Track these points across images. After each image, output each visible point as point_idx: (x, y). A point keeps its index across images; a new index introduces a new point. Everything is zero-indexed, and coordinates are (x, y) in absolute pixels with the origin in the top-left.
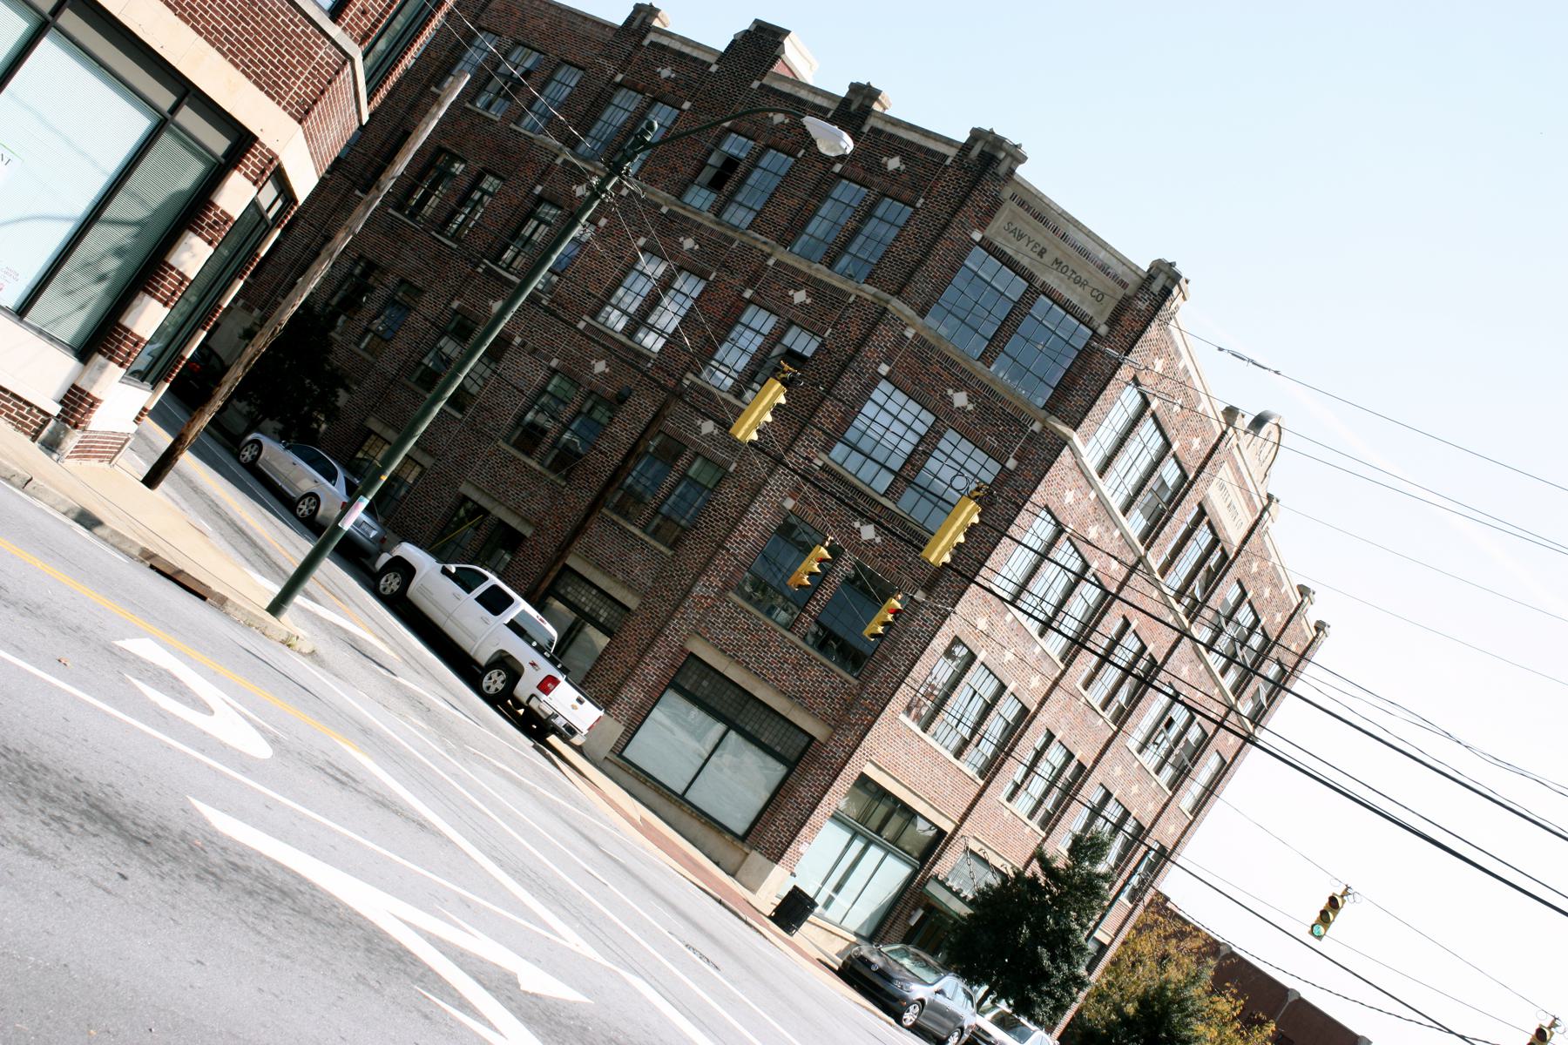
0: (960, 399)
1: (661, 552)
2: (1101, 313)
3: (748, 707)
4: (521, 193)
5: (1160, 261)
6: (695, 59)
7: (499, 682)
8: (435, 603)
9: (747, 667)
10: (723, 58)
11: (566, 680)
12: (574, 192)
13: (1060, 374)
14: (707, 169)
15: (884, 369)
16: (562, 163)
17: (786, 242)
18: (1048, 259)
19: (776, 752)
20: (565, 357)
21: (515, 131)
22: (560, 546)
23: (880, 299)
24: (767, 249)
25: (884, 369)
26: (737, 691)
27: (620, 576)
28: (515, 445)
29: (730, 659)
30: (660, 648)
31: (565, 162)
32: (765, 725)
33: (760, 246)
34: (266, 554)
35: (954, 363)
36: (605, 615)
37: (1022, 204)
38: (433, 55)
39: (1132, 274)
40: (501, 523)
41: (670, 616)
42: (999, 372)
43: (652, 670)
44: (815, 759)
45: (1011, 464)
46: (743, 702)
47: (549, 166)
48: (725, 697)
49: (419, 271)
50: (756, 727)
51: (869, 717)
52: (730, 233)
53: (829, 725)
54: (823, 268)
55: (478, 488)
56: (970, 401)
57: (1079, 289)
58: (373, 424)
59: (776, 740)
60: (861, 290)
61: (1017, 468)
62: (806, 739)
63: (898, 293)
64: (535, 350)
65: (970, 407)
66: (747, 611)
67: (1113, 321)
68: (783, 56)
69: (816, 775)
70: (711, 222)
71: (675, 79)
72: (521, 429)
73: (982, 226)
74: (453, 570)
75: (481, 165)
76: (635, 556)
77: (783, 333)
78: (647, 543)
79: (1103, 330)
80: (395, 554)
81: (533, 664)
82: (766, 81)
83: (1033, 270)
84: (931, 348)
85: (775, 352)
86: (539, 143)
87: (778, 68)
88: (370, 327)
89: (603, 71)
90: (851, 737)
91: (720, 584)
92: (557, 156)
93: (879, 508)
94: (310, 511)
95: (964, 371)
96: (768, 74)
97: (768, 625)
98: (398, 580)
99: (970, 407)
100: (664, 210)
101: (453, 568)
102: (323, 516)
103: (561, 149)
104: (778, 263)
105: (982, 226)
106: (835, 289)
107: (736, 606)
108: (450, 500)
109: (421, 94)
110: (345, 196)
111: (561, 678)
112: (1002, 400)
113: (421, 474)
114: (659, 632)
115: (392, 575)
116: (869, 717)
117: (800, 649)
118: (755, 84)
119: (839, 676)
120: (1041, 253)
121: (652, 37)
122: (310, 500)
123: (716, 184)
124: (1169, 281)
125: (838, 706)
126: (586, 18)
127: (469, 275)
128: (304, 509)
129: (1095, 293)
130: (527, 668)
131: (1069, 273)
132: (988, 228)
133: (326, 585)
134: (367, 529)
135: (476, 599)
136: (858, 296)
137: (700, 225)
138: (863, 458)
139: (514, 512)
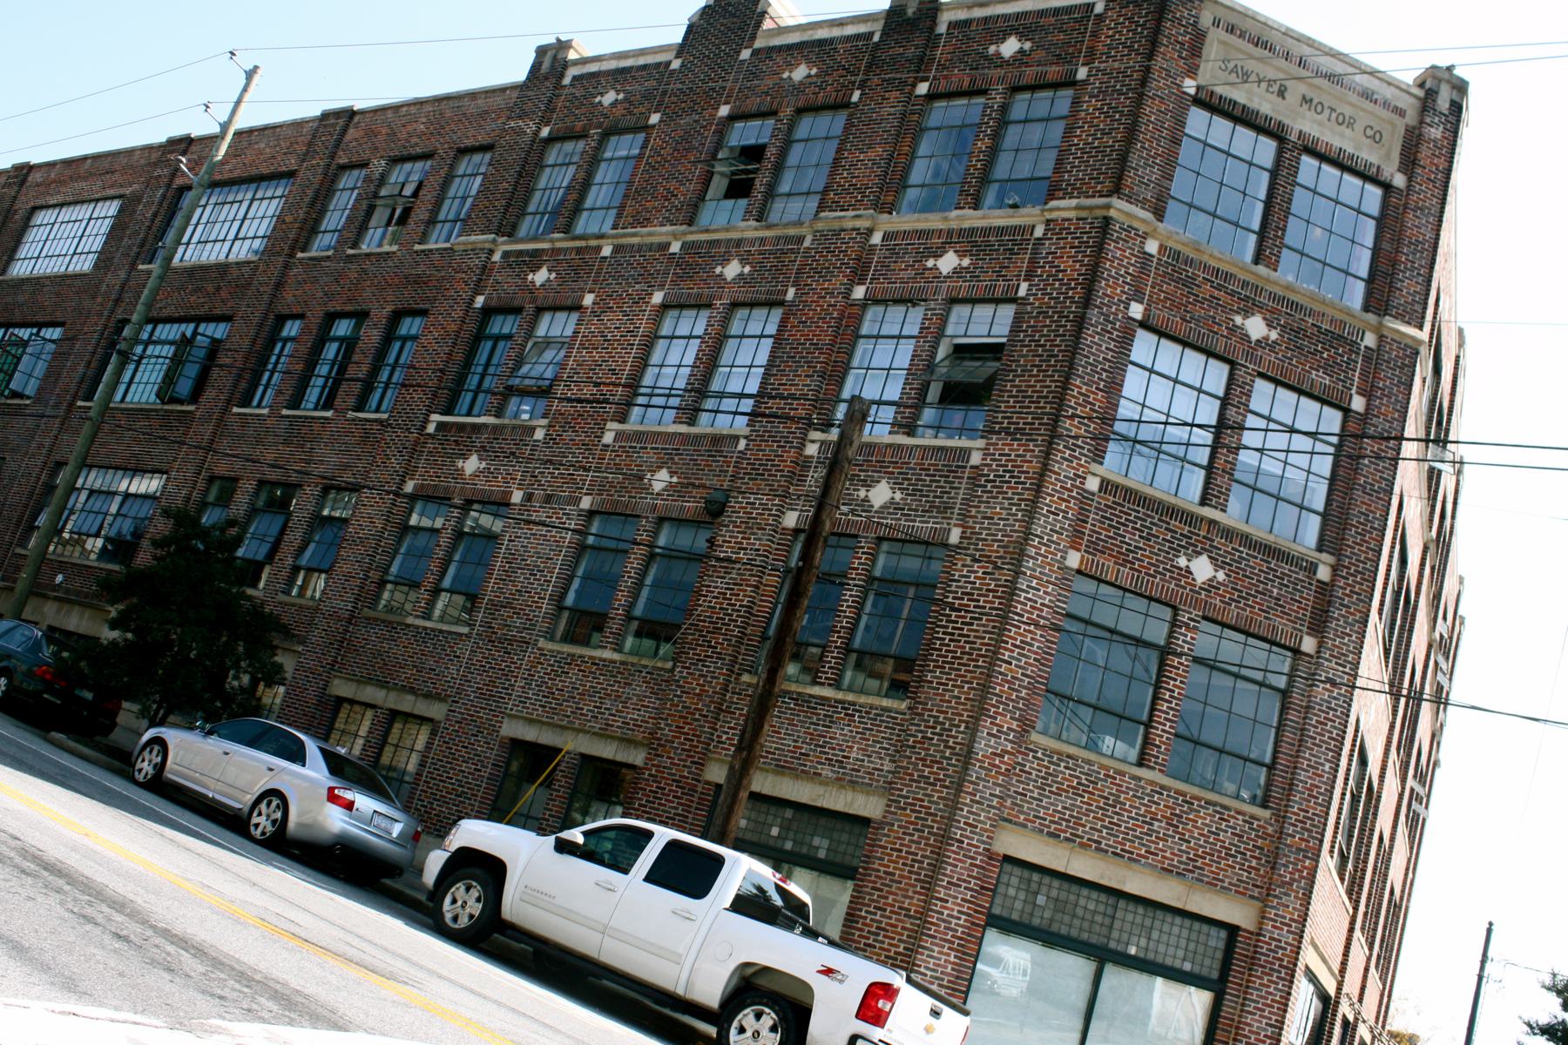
0: (1256, 327)
1: (885, 709)
2: (1388, 156)
3: (1119, 914)
4: (458, 313)
5: (1434, 67)
6: (645, 67)
7: (765, 1032)
8: (567, 915)
9: (1098, 849)
10: (681, 50)
11: (909, 980)
12: (533, 282)
13: (1366, 256)
14: (716, 178)
15: (1136, 311)
16: (502, 257)
17: (887, 207)
18: (1293, 97)
19: (1130, 957)
20: (598, 489)
21: (423, 251)
22: (741, 741)
23: (1091, 208)
24: (863, 224)
25: (1136, 311)
26: (1103, 897)
27: (826, 772)
28: (568, 638)
29: (1065, 844)
30: (957, 867)
31: (506, 254)
32: (1155, 935)
33: (849, 224)
34: (120, 905)
35: (1228, 276)
36: (825, 843)
37: (1231, 29)
38: (288, 219)
39: (1403, 94)
40: (586, 759)
41: (954, 806)
42: (1288, 274)
43: (953, 907)
44: (1252, 961)
45: (1358, 403)
46: (1110, 911)
47: (484, 267)
48: (1080, 912)
49: (346, 467)
50: (1143, 942)
51: (1307, 862)
52: (792, 232)
53: (1252, 897)
54: (968, 212)
55: (531, 721)
56: (1270, 326)
57: (1348, 132)
58: (342, 688)
59: (1180, 953)
60: (1051, 210)
61: (1368, 407)
62: (1223, 934)
63: (1116, 190)
64: (548, 499)
65: (1274, 335)
66: (1069, 756)
67: (1409, 163)
68: (769, 10)
69: (1263, 987)
70: (756, 229)
71: (625, 99)
72: (566, 614)
73: (1192, 72)
74: (580, 840)
75: (389, 308)
76: (840, 732)
77: (944, 321)
78: (851, 704)
79: (1399, 181)
80: (453, 848)
81: (828, 972)
82: (758, 44)
83: (1279, 118)
84: (1189, 262)
85: (942, 353)
86: (462, 247)
87: (767, 24)
88: (297, 563)
89: (523, 133)
90: (1293, 903)
91: (1014, 725)
92: (491, 252)
93: (1205, 527)
94: (274, 822)
95: (1245, 284)
96: (759, 33)
97: (1107, 768)
98: (475, 893)
99: (1274, 335)
100: (675, 247)
101: (576, 835)
102: (299, 825)
103: (494, 241)
104: (886, 237)
105: (1192, 72)
106: (1001, 231)
107: (1049, 753)
108: (492, 755)
109: (286, 266)
110: (221, 419)
111: (897, 979)
112: (1311, 313)
113: (433, 733)
114: (945, 838)
115: (461, 886)
116: (1307, 862)
117: (1169, 790)
118: (745, 54)
119: (1239, 813)
120: (1281, 93)
121: (572, 72)
122: (269, 805)
123: (738, 188)
124: (1455, 92)
125: (1254, 863)
126: (473, 95)
127: (417, 442)
128: (262, 822)
129: (1369, 132)
130: (819, 984)
131: (1327, 112)
132: (1200, 72)
133: (342, 948)
134: (384, 823)
135: (648, 879)
136: (1048, 222)
137: (739, 243)
138: (1139, 438)
139: (604, 735)
